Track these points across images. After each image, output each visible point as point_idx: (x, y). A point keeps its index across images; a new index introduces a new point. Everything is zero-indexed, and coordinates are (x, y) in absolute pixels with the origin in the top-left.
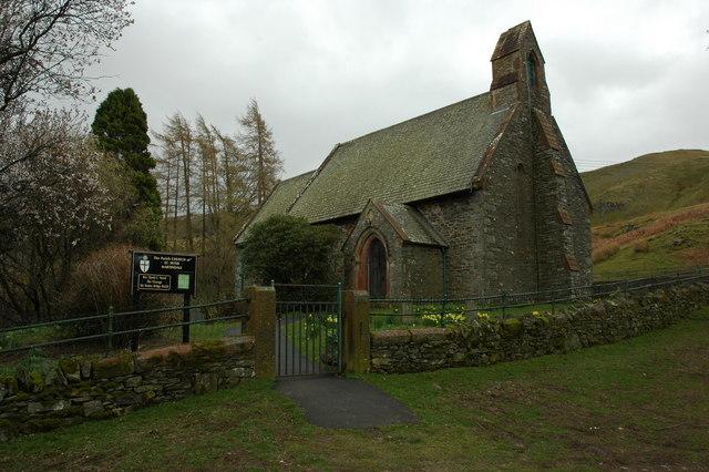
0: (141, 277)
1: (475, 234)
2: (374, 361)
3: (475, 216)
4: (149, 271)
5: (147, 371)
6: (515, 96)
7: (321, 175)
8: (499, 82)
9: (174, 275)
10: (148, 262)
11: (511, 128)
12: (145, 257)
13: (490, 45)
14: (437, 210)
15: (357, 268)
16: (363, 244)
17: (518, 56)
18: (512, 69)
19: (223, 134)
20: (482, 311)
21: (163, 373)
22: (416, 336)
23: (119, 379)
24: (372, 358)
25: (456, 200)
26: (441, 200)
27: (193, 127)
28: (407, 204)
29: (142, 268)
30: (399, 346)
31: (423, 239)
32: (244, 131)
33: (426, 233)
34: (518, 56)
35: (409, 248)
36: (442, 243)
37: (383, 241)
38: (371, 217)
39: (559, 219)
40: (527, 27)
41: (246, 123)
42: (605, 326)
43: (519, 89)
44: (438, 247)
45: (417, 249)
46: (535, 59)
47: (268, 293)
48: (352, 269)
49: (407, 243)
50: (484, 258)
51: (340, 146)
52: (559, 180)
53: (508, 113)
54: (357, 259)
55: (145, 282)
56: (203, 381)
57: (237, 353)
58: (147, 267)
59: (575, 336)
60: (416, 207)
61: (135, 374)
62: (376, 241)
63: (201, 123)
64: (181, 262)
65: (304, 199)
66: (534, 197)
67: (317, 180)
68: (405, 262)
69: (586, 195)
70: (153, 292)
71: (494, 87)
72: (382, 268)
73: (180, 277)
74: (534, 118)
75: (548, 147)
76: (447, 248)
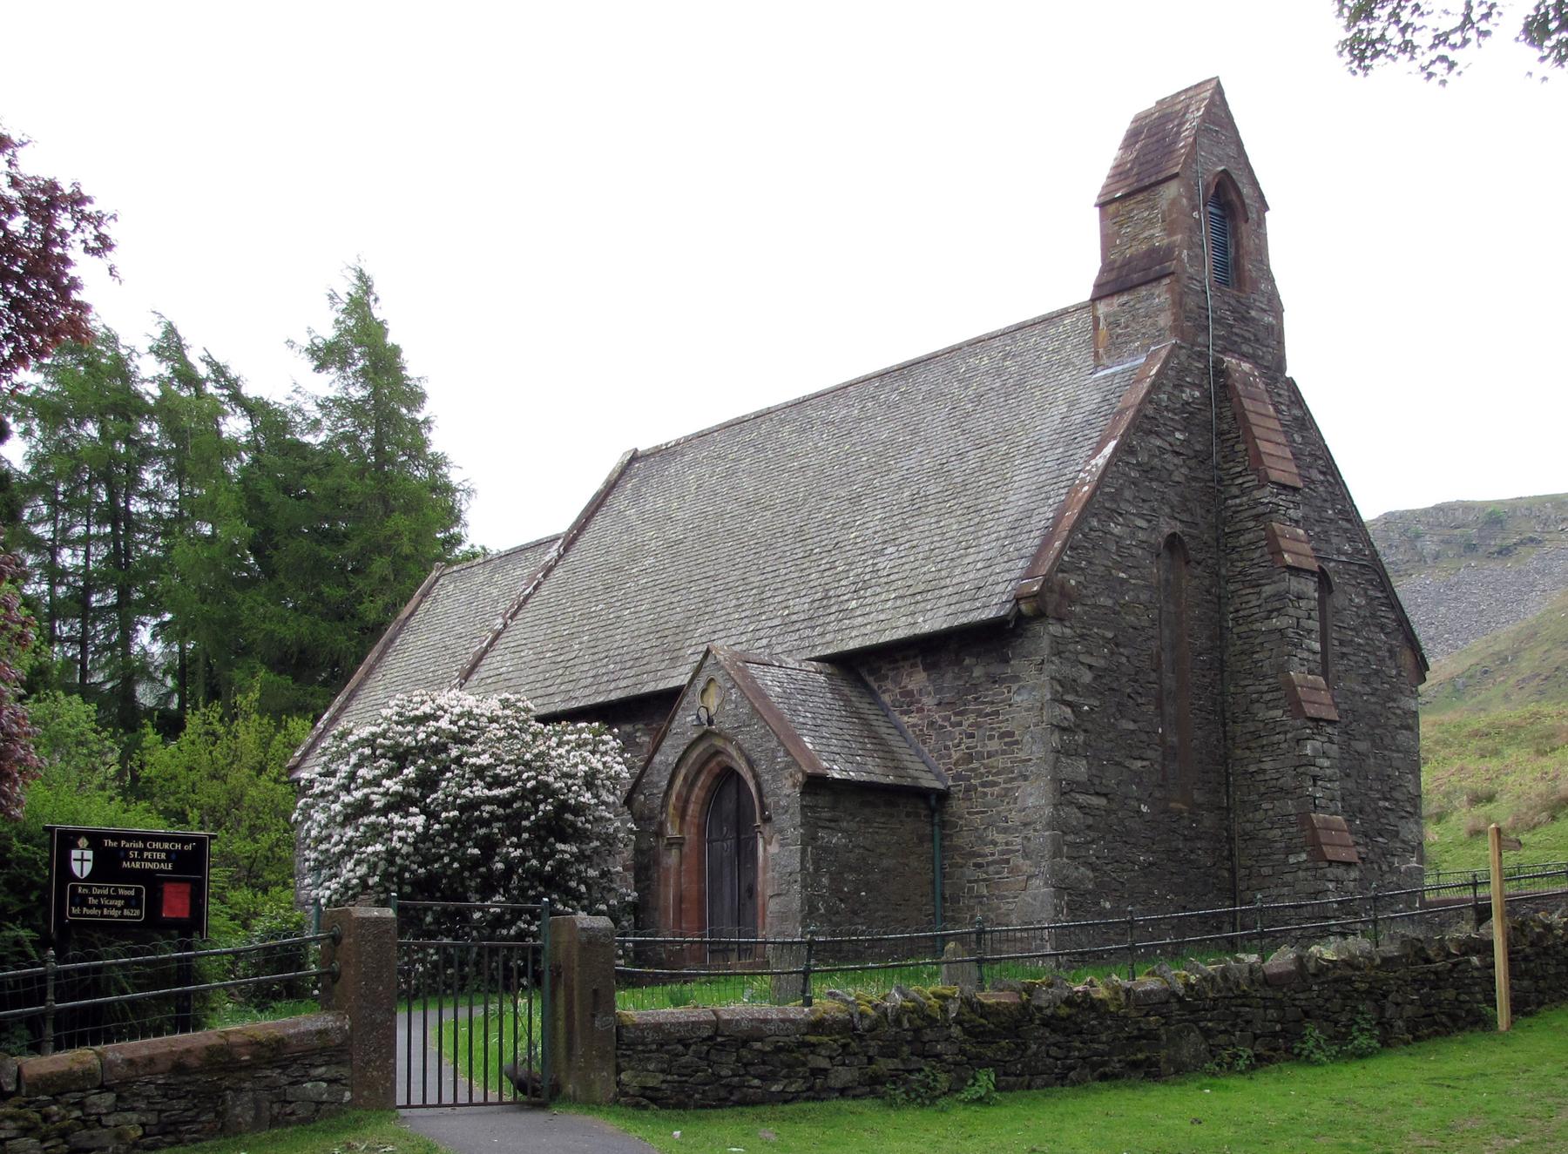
0: (74, 888)
1: (1015, 765)
3: (1027, 699)
4: (93, 876)
5: (126, 1082)
7: (572, 557)
8: (1118, 280)
10: (89, 854)
11: (1144, 423)
12: (83, 842)
13: (1098, 156)
14: (917, 680)
15: (672, 859)
16: (690, 784)
17: (1189, 206)
19: (249, 391)
21: (158, 1087)
22: (728, 1022)
23: (72, 1097)
24: (619, 1071)
27: (149, 373)
28: (819, 659)
29: (76, 867)
30: (687, 1046)
31: (871, 770)
32: (327, 385)
34: (1189, 206)
35: (823, 800)
37: (748, 776)
41: (326, 356)
43: (1179, 303)
44: (921, 794)
46: (1232, 205)
47: (378, 921)
49: (816, 784)
51: (635, 457)
52: (1295, 585)
54: (672, 831)
55: (82, 901)
56: (241, 1109)
58: (88, 867)
60: (857, 669)
61: (103, 1088)
62: (729, 776)
63: (170, 347)
64: (168, 852)
65: (519, 631)
67: (558, 572)
68: (809, 840)
71: (1106, 288)
72: (745, 853)
73: (169, 889)
74: (1223, 389)
76: (943, 796)
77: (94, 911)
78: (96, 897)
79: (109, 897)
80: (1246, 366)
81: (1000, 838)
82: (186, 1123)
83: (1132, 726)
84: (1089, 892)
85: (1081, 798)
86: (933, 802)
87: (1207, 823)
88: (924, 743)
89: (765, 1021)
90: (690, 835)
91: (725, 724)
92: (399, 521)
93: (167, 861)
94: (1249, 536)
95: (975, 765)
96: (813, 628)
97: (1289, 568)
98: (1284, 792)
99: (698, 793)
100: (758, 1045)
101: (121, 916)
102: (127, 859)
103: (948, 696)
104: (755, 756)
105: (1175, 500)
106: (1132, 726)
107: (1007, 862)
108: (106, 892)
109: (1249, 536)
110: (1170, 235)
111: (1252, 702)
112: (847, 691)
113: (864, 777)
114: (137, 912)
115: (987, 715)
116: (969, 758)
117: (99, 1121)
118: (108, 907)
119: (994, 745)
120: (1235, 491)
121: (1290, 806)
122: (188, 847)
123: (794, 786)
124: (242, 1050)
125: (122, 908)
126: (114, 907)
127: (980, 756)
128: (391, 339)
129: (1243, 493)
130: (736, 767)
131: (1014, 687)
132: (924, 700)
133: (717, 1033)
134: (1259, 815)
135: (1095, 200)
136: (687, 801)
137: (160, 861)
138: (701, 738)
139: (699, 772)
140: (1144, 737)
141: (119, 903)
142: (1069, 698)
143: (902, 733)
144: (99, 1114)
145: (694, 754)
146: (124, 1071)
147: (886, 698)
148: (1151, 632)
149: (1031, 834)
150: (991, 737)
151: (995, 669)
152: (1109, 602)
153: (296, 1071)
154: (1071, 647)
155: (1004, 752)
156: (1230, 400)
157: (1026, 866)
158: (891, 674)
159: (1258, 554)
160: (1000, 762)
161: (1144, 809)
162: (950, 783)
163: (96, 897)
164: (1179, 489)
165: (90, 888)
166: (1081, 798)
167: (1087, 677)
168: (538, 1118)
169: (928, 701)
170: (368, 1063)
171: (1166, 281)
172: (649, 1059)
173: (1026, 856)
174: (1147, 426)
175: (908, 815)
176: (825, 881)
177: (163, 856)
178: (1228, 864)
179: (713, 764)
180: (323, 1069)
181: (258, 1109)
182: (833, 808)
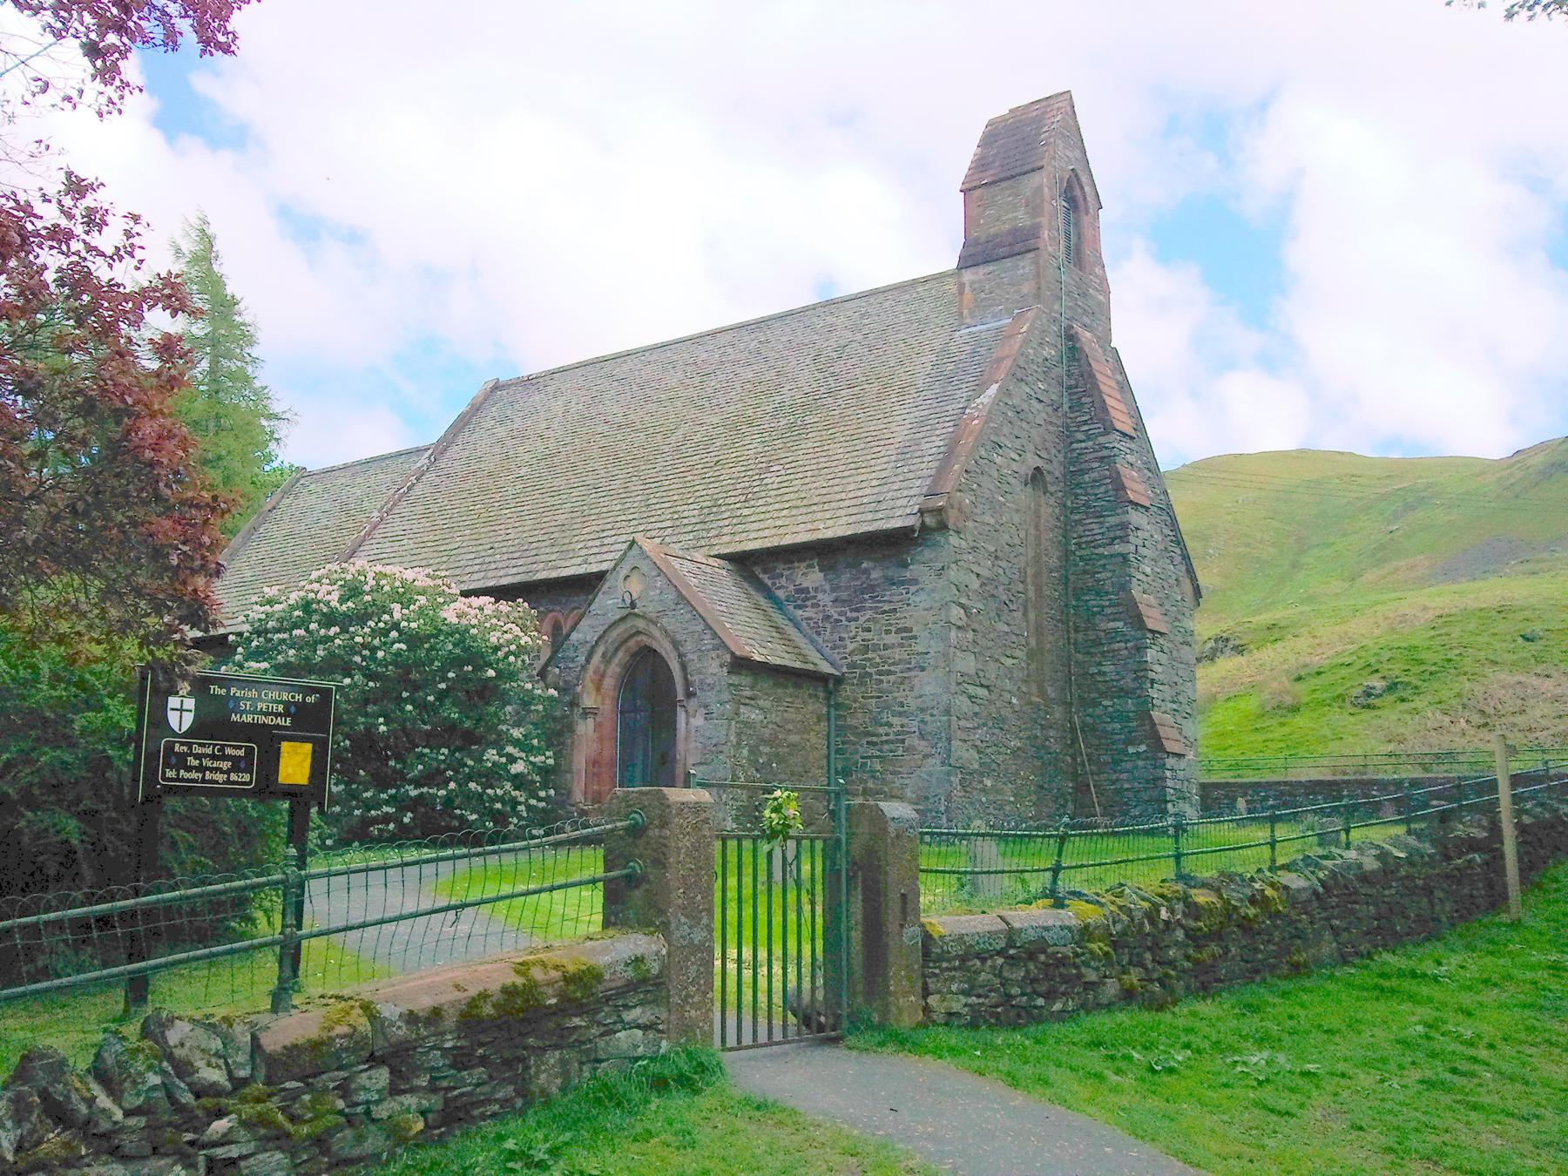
0: (170, 747)
2: (933, 1000)
4: (192, 732)
6: (1026, 288)
9: (267, 742)
10: (190, 703)
14: (812, 577)
15: (585, 728)
18: (1022, 218)
20: (698, 808)
23: (329, 1080)
24: (926, 992)
25: (876, 554)
26: (825, 552)
28: (718, 556)
29: (173, 718)
30: (984, 960)
31: (777, 655)
33: (787, 640)
34: (1029, 190)
36: (826, 668)
38: (635, 587)
39: (1138, 621)
40: (1062, 104)
42: (1384, 907)
45: (766, 684)
48: (570, 728)
49: (741, 664)
50: (947, 712)
51: (497, 387)
52: (1135, 517)
53: (1002, 336)
54: (588, 701)
56: (546, 1073)
57: (631, 987)
58: (188, 719)
59: (1327, 935)
60: (747, 565)
61: (374, 1060)
64: (287, 704)
66: (1067, 554)
69: (1186, 558)
70: (208, 793)
74: (1073, 350)
75: (1109, 428)
76: (839, 680)
77: (194, 775)
78: (197, 756)
79: (213, 757)
80: (1088, 334)
81: (895, 721)
82: (483, 1103)
83: (1006, 629)
84: (975, 771)
85: (972, 690)
86: (831, 686)
87: (1057, 715)
88: (819, 634)
89: (1047, 929)
90: (607, 707)
91: (647, 607)
92: (227, 441)
93: (286, 714)
94: (1094, 475)
95: (870, 655)
96: (708, 531)
97: (1131, 502)
98: (1125, 693)
99: (615, 668)
100: (1042, 958)
101: (228, 782)
102: (236, 710)
103: (844, 595)
104: (678, 637)
105: (1038, 440)
106: (1006, 629)
107: (903, 741)
108: (209, 751)
109: (1094, 475)
110: (1033, 217)
111: (1094, 614)
112: (746, 585)
113: (778, 662)
114: (247, 778)
115: (884, 612)
116: (866, 649)
117: (368, 1113)
118: (211, 770)
119: (892, 639)
120: (1080, 436)
121: (1130, 704)
122: (311, 699)
123: (721, 666)
124: (550, 991)
125: (228, 772)
126: (217, 769)
127: (876, 648)
128: (229, 290)
129: (1089, 438)
130: (655, 646)
131: (913, 589)
132: (820, 596)
133: (1011, 943)
134: (1099, 711)
135: (960, 186)
136: (603, 676)
137: (277, 715)
138: (622, 619)
139: (617, 650)
140: (1014, 639)
141: (226, 765)
142: (963, 601)
143: (797, 626)
144: (368, 1102)
145: (614, 634)
146: (402, 1032)
147: (781, 594)
148: (1021, 550)
149: (928, 718)
150: (888, 632)
151: (893, 572)
152: (992, 521)
153: (606, 1016)
154: (965, 557)
155: (902, 645)
156: (1078, 360)
157: (922, 746)
158: (786, 573)
159: (1103, 489)
160: (897, 654)
161: (1014, 701)
162: (845, 670)
163: (197, 756)
164: (1041, 430)
165: (190, 745)
166: (972, 690)
167: (975, 584)
168: (828, 1053)
169: (825, 598)
170: (685, 1000)
171: (1031, 255)
172: (953, 978)
173: (922, 737)
174: (1019, 375)
175: (810, 696)
176: (745, 752)
177: (281, 708)
178: (1071, 751)
179: (631, 643)
180: (638, 1010)
181: (566, 1075)
182: (752, 688)
